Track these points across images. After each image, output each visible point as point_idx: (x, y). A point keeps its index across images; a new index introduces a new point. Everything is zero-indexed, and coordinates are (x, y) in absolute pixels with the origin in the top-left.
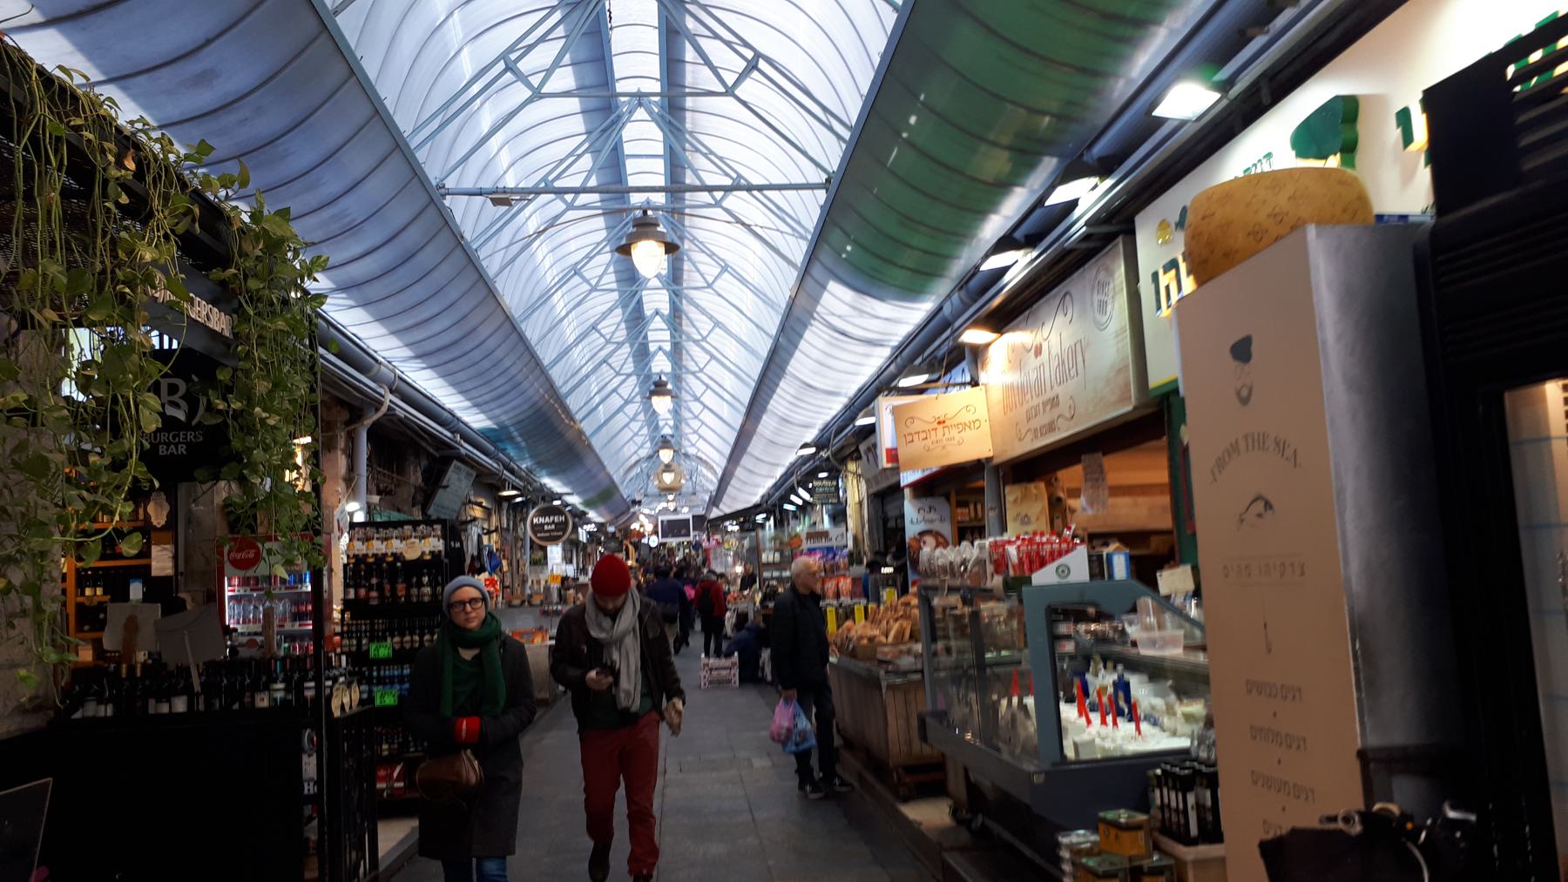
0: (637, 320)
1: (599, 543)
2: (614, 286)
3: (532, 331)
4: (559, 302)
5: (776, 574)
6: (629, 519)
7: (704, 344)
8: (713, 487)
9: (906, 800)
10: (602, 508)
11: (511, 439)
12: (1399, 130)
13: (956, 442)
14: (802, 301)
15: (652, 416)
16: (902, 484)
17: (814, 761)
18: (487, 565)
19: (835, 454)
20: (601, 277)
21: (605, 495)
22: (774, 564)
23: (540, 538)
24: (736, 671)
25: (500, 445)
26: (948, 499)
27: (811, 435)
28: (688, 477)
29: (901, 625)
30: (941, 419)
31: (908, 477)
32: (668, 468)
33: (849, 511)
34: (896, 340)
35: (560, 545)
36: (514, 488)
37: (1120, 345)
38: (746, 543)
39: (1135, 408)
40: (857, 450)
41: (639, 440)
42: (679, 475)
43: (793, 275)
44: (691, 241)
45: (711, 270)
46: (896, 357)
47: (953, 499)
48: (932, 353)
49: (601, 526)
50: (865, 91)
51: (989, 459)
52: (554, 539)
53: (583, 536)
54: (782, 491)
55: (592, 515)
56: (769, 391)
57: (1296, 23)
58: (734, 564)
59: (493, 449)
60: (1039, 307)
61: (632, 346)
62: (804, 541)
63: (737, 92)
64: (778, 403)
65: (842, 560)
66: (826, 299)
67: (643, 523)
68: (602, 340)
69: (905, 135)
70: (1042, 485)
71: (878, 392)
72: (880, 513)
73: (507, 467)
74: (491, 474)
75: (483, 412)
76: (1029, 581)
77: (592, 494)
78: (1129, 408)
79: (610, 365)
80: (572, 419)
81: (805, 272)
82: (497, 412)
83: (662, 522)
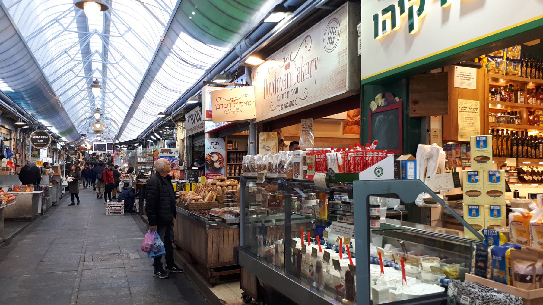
0: (87, 52)
1: (67, 151)
2: (76, 30)
3: (32, 45)
4: (48, 34)
5: (143, 167)
6: (81, 142)
7: (116, 66)
8: (117, 132)
9: (214, 285)
10: (68, 136)
11: (23, 98)
12: (399, 7)
13: (239, 110)
14: (125, 123)
15: (92, 98)
16: (205, 131)
17: (163, 260)
18: (5, 155)
19: (174, 118)
20: (76, 54)
21: (70, 130)
22: (143, 163)
23: (35, 145)
24: (123, 208)
25: (17, 101)
26: (224, 140)
27: (163, 110)
28: (106, 127)
29: (212, 194)
30: (233, 99)
31: (210, 126)
32: (98, 122)
33: (177, 143)
34: (208, 66)
35: (47, 148)
36: (23, 121)
37: (341, 59)
38: (130, 155)
39: (348, 92)
40: (184, 117)
41: (86, 108)
42: (103, 125)
43: (162, 31)
44: (111, 46)
45: (118, 57)
46: (208, 74)
47: (227, 139)
48: (229, 69)
49: (68, 144)
50: (157, 46)
51: (253, 120)
52: (43, 146)
53: (59, 146)
54: (147, 134)
55: (63, 138)
56: (140, 99)
57: (313, 3)
58: (124, 163)
59: (12, 102)
60: (289, 45)
61: (81, 46)
62: (160, 153)
63: (119, 63)
64: (149, 94)
65: (176, 163)
66: (178, 42)
67: (88, 144)
68: (69, 58)
69: (190, 18)
70: (276, 133)
71: (205, 83)
72: (192, 145)
73: (19, 111)
74: (11, 113)
75: (6, 83)
76: (357, 177)
77: (64, 130)
78: (345, 91)
79: (80, 96)
80: (55, 95)
81: (169, 29)
82: (15, 83)
83: (95, 144)
